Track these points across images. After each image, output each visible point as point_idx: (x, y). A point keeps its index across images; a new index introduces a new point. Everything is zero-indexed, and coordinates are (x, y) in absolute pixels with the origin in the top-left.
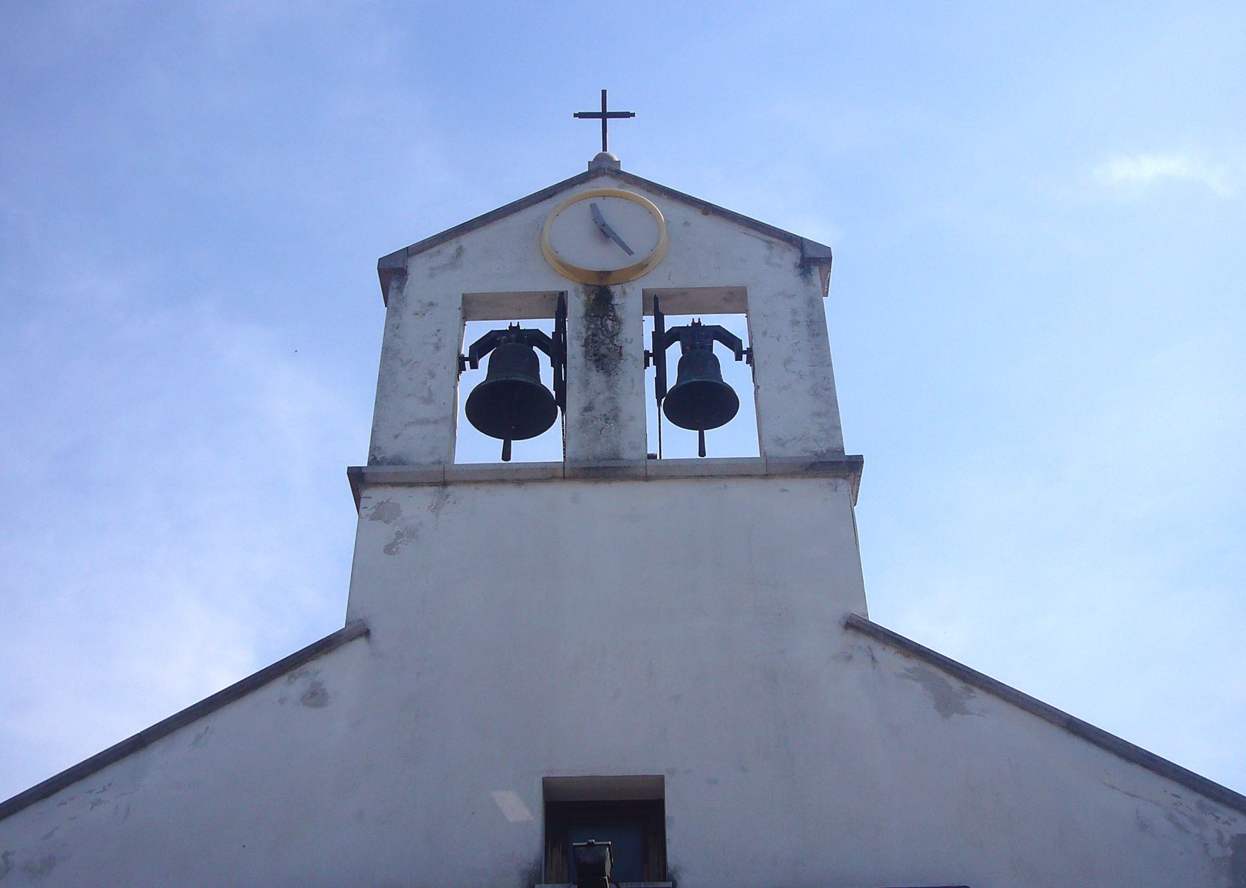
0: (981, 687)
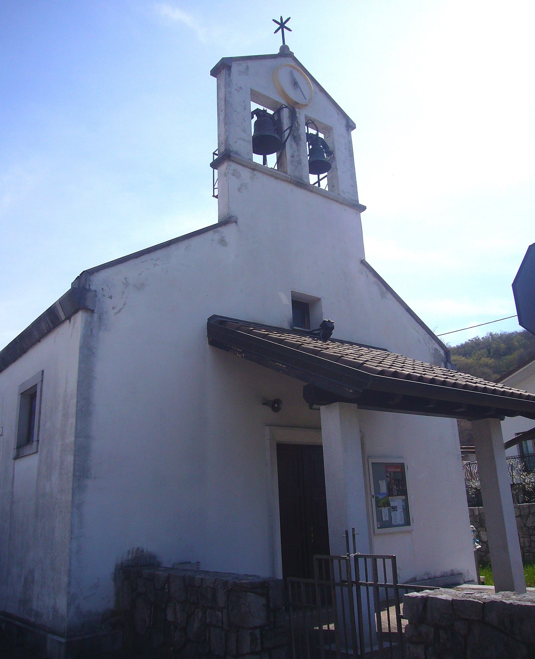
0: (390, 292)
